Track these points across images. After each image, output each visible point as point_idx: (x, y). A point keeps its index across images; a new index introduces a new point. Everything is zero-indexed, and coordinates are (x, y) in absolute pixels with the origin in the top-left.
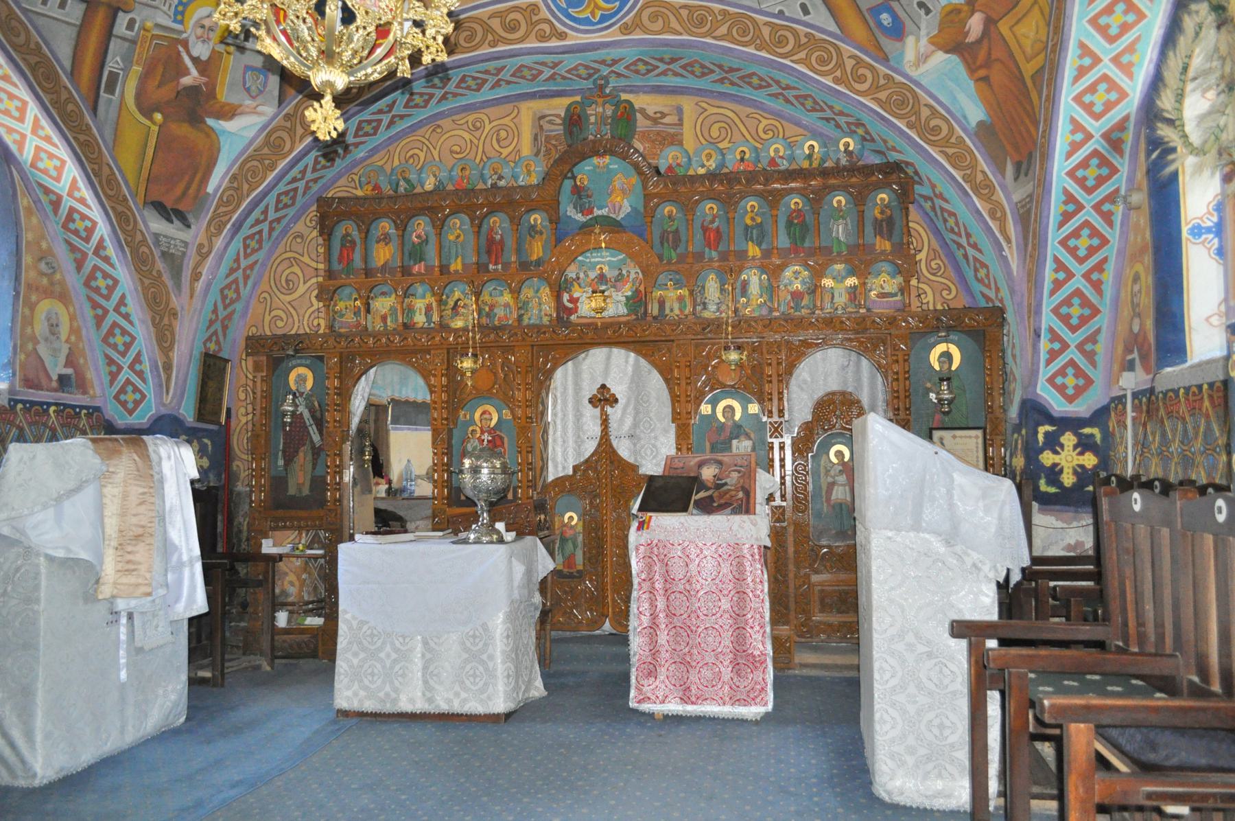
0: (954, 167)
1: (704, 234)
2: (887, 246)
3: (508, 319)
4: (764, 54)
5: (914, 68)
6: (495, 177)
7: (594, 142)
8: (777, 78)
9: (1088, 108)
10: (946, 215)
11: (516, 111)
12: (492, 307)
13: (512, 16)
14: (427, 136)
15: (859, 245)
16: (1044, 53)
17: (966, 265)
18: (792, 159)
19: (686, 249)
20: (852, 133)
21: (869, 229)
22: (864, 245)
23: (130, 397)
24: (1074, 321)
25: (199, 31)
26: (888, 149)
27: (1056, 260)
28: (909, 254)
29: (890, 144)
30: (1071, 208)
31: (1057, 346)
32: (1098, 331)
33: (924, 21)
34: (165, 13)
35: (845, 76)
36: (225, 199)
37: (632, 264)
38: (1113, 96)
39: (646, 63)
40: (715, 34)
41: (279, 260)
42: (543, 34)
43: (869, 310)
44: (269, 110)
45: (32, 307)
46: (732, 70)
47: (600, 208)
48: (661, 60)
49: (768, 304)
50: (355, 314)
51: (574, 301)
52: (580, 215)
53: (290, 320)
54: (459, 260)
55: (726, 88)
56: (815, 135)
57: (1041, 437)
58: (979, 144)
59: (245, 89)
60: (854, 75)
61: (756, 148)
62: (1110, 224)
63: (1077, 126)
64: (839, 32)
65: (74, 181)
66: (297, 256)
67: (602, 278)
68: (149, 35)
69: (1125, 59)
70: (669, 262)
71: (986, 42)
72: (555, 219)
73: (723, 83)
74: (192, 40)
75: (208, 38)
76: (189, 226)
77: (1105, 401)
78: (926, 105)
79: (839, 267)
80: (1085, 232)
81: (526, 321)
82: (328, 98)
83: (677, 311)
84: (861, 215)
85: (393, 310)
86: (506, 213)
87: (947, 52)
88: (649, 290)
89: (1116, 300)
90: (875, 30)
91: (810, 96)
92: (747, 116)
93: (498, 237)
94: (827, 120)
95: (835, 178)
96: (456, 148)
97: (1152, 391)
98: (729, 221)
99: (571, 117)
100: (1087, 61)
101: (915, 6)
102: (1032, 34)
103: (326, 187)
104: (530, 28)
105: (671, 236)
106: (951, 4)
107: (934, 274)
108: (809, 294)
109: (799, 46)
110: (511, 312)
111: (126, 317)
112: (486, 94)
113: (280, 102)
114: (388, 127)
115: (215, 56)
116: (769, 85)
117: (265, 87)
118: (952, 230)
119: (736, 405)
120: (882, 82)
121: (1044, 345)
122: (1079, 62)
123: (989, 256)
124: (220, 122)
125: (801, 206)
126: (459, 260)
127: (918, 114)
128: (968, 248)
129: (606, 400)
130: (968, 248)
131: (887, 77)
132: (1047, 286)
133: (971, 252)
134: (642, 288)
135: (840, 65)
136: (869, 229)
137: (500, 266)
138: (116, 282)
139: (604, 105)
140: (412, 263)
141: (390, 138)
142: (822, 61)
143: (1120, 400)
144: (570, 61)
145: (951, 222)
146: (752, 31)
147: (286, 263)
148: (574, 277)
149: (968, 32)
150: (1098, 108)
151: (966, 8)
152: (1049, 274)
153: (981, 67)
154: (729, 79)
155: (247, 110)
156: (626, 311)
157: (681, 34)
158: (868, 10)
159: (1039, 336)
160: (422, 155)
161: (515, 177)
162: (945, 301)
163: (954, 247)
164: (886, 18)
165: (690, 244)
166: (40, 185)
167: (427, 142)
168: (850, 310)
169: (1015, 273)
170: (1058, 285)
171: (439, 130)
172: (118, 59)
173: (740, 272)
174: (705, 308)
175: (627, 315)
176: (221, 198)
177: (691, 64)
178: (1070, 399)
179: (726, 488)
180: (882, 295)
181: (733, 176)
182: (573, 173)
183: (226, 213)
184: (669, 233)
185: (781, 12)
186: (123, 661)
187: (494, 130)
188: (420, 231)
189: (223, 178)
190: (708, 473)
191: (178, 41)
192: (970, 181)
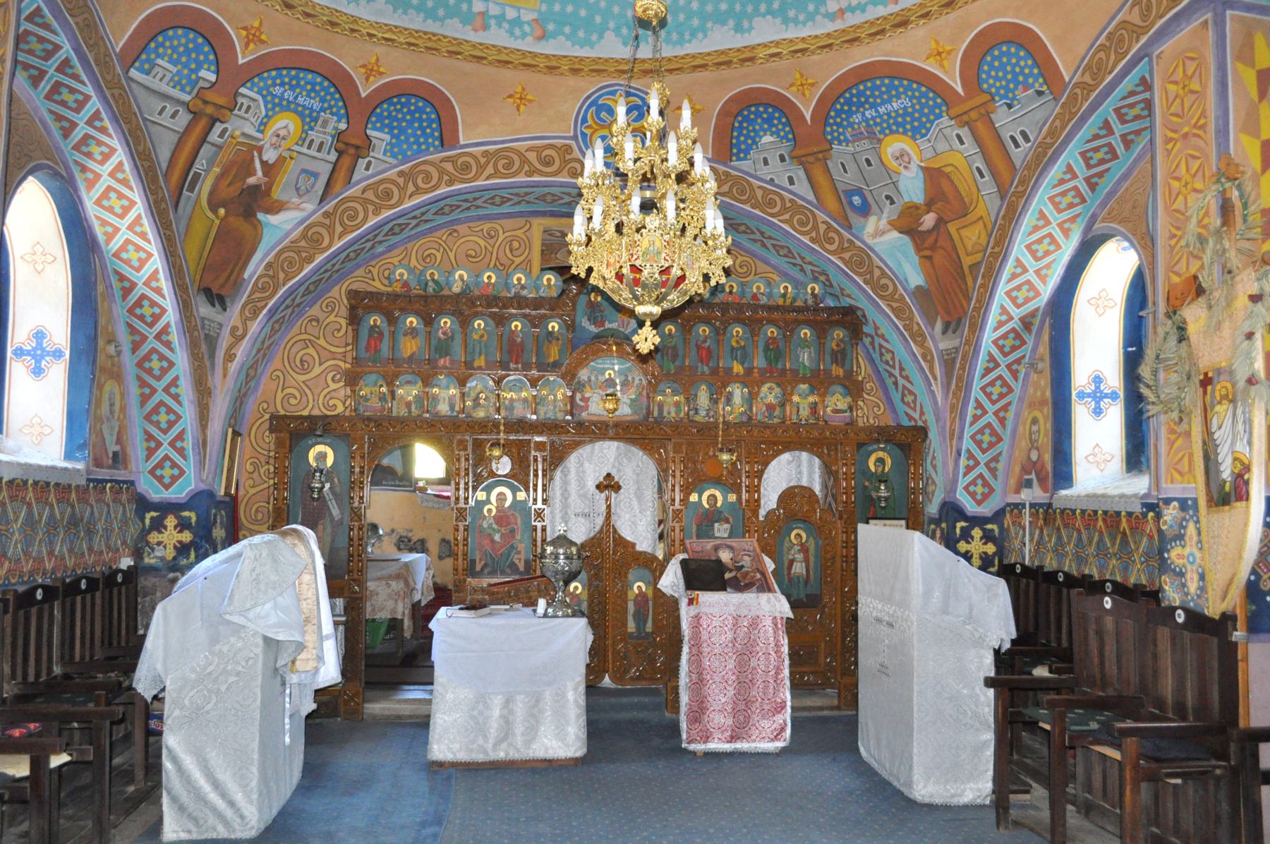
0: (896, 316)
1: (698, 352)
4: (757, 212)
9: (1014, 300)
16: (981, 254)
18: (770, 295)
19: (684, 363)
20: (815, 279)
23: (167, 472)
24: (985, 446)
25: (275, 139)
27: (977, 401)
29: (759, 244)
30: (992, 365)
31: (971, 463)
32: (1000, 454)
33: (887, 207)
34: (252, 124)
36: (260, 286)
37: (637, 373)
38: (1031, 294)
44: (310, 207)
45: (101, 388)
47: (611, 322)
50: (380, 399)
53: (304, 399)
54: (483, 357)
56: (785, 276)
57: (958, 531)
62: (1016, 379)
63: (1004, 310)
64: (815, 201)
65: (156, 271)
66: (312, 338)
68: (235, 142)
69: (1044, 272)
74: (267, 146)
76: (225, 310)
77: (1002, 505)
80: (999, 383)
82: (648, 323)
83: (673, 414)
87: (901, 232)
88: (651, 395)
89: (1014, 431)
93: (519, 340)
96: (473, 253)
97: (1049, 505)
100: (1019, 270)
102: (974, 239)
109: (784, 209)
111: (176, 398)
113: (321, 201)
115: (281, 160)
117: (312, 188)
118: (887, 363)
119: (718, 494)
120: (846, 245)
121: (963, 462)
122: (1013, 270)
126: (483, 357)
127: (871, 273)
129: (612, 487)
131: (850, 241)
132: (969, 419)
135: (816, 227)
138: (172, 364)
143: (1019, 506)
145: (888, 357)
150: (1020, 301)
151: (924, 208)
152: (971, 411)
153: (926, 248)
159: (960, 455)
160: (439, 256)
162: (876, 417)
163: (885, 375)
164: (857, 200)
166: (117, 273)
168: (811, 421)
170: (976, 418)
171: (455, 235)
172: (204, 162)
173: (725, 386)
174: (697, 413)
176: (256, 283)
178: (979, 503)
179: (744, 570)
180: (836, 411)
183: (260, 300)
184: (668, 348)
185: (772, 180)
186: (287, 727)
188: (1095, 472)
189: (258, 265)
190: (725, 556)
191: (255, 147)
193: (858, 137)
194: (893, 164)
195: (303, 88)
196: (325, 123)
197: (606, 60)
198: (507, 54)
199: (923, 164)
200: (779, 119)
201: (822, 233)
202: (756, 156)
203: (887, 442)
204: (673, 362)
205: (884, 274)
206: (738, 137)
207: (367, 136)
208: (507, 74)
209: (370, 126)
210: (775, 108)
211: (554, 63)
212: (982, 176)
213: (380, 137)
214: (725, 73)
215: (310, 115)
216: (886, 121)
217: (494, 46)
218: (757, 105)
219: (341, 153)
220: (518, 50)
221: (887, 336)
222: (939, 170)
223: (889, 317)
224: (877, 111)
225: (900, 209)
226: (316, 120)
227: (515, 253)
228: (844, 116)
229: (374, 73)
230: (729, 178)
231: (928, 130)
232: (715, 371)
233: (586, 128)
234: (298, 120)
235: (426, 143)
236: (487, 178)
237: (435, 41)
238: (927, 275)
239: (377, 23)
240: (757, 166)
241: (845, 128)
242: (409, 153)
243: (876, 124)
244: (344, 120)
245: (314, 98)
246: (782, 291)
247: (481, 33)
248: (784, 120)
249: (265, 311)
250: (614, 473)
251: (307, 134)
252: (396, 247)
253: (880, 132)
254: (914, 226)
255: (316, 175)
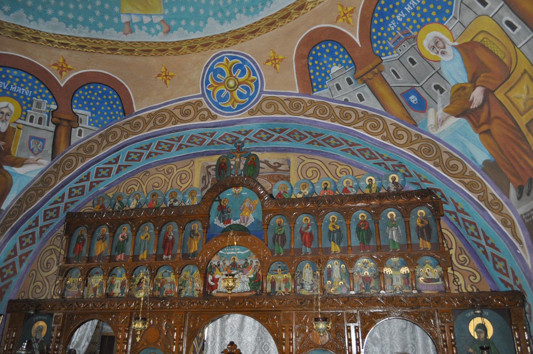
1: (302, 236)
2: (428, 245)
3: (171, 292)
5: (434, 129)
6: (172, 200)
7: (233, 178)
8: (346, 138)
10: (467, 224)
11: (192, 163)
12: (162, 284)
13: (186, 108)
14: (140, 178)
15: (408, 245)
17: (486, 260)
20: (396, 172)
21: (414, 233)
22: (411, 244)
26: (422, 181)
28: (444, 251)
33: (440, 97)
35: (389, 135)
36: (11, 213)
37: (254, 256)
39: (266, 133)
40: (306, 114)
41: (45, 250)
42: (203, 116)
43: (419, 291)
46: (318, 135)
47: (235, 219)
48: (274, 130)
49: (347, 285)
51: (215, 280)
52: (222, 224)
55: (315, 147)
56: (372, 173)
58: (486, 176)
59: (30, 149)
60: (395, 135)
61: (335, 182)
64: (383, 110)
67: (234, 265)
70: (279, 254)
71: (486, 108)
72: (207, 226)
73: (313, 144)
75: (6, 120)
78: (445, 152)
79: (395, 259)
81: (183, 294)
83: (283, 289)
84: (407, 223)
85: (101, 284)
86: (176, 222)
90: (407, 107)
91: (368, 149)
92: (329, 164)
94: (380, 164)
95: (388, 200)
96: (157, 185)
98: (318, 228)
99: (220, 165)
101: (433, 88)
102: (524, 96)
103: (80, 207)
104: (196, 113)
105: (280, 237)
106: (458, 84)
107: (462, 265)
108: (375, 279)
109: (358, 119)
110: (174, 288)
112: (174, 154)
113: (53, 158)
114: (117, 172)
116: (341, 144)
117: (43, 148)
118: (473, 234)
120: (414, 138)
123: (505, 252)
124: (13, 168)
125: (366, 218)
126: (145, 253)
127: (440, 157)
128: (486, 247)
130: (486, 247)
133: (489, 250)
134: (260, 273)
135: (386, 129)
136: (414, 233)
137: (170, 257)
139: (240, 157)
140: (117, 253)
141: (119, 179)
142: (374, 127)
144: (220, 132)
146: (328, 111)
147: (49, 252)
148: (216, 264)
149: (472, 101)
151: (469, 85)
153: (483, 124)
154: (316, 141)
155: (32, 161)
156: (249, 288)
157: (285, 114)
158: (401, 94)
161: (184, 201)
163: (475, 246)
164: (413, 99)
165: (292, 242)
167: (140, 181)
168: (405, 291)
169: (530, 267)
171: (148, 174)
173: (326, 263)
174: (302, 288)
175: (250, 291)
177: (293, 133)
180: (428, 280)
181: (319, 199)
182: (219, 198)
184: (279, 235)
185: (346, 100)
187: (180, 173)
188: (124, 233)
189: (14, 200)
192: (484, 200)
193: (398, 43)
194: (431, 54)
195: (12, 80)
196: (39, 105)
197: (211, 37)
198: (148, 46)
199: (456, 44)
200: (338, 50)
201: (391, 132)
202: (331, 85)
203: (482, 307)
204: (283, 247)
205: (452, 157)
206: (314, 73)
207: (74, 113)
208: (153, 61)
209: (74, 106)
210: (334, 42)
211: (178, 46)
212: (513, 28)
213: (84, 114)
214: (290, 24)
215: (25, 99)
216: (415, 17)
217: (139, 42)
218: (319, 44)
219: (57, 125)
220: (155, 42)
221: (466, 210)
222: (472, 42)
223: (463, 191)
224: (405, 12)
225: (449, 94)
226: (31, 102)
227: (182, 182)
228: (382, 29)
229: (64, 69)
230: (313, 104)
231: (451, 8)
232: (315, 251)
233: (209, 87)
234: (16, 103)
235: (114, 114)
236: (149, 130)
237: (99, 44)
238: (489, 147)
239: (54, 34)
240: (333, 92)
241: (386, 39)
242: (105, 122)
243: (408, 24)
244: (53, 103)
245: (24, 87)
246: (368, 183)
247: (130, 35)
248: (342, 50)
249: (9, 230)
250: (236, 343)
251: (27, 112)
252: (112, 186)
253: (413, 30)
254: (466, 106)
255: (43, 140)
